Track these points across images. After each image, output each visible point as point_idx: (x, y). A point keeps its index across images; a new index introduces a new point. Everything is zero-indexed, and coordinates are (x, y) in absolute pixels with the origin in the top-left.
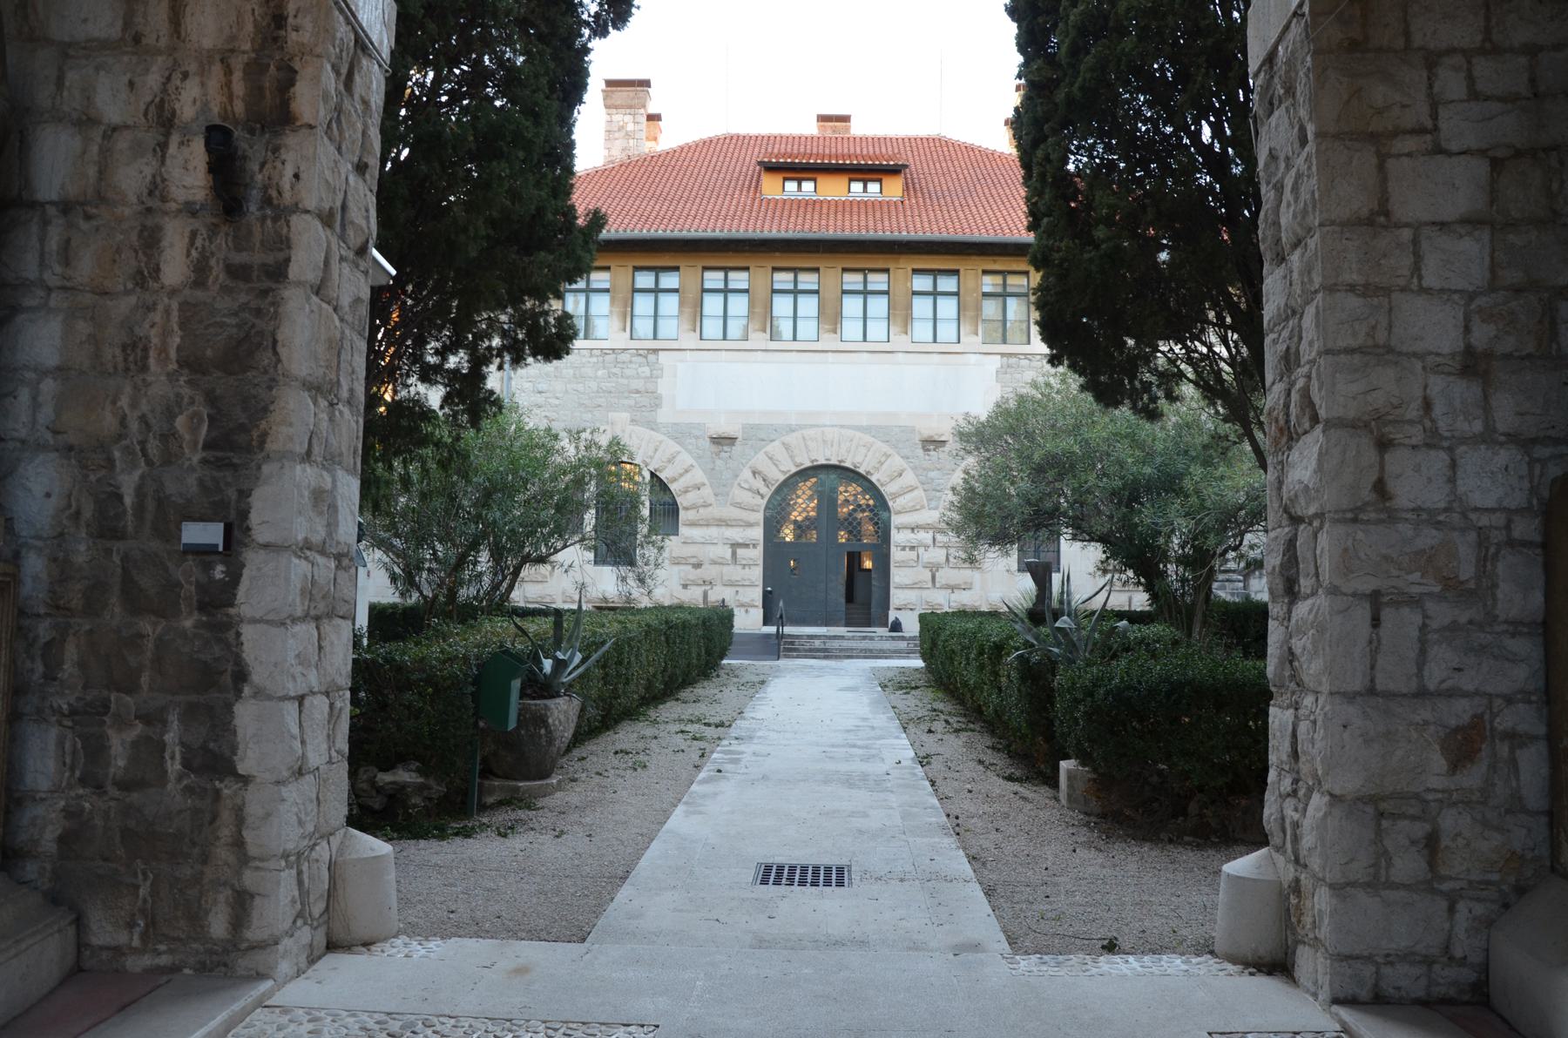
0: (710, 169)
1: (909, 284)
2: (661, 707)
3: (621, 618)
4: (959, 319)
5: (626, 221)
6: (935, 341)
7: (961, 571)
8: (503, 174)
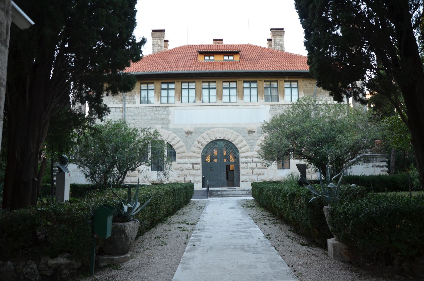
0: (183, 54)
1: (242, 85)
2: (172, 217)
3: (157, 187)
4: (257, 95)
5: (159, 69)
6: (251, 102)
7: (261, 169)
8: (104, 14)
